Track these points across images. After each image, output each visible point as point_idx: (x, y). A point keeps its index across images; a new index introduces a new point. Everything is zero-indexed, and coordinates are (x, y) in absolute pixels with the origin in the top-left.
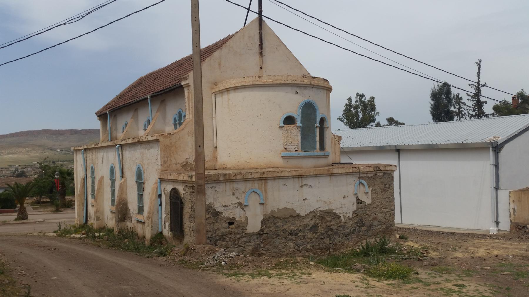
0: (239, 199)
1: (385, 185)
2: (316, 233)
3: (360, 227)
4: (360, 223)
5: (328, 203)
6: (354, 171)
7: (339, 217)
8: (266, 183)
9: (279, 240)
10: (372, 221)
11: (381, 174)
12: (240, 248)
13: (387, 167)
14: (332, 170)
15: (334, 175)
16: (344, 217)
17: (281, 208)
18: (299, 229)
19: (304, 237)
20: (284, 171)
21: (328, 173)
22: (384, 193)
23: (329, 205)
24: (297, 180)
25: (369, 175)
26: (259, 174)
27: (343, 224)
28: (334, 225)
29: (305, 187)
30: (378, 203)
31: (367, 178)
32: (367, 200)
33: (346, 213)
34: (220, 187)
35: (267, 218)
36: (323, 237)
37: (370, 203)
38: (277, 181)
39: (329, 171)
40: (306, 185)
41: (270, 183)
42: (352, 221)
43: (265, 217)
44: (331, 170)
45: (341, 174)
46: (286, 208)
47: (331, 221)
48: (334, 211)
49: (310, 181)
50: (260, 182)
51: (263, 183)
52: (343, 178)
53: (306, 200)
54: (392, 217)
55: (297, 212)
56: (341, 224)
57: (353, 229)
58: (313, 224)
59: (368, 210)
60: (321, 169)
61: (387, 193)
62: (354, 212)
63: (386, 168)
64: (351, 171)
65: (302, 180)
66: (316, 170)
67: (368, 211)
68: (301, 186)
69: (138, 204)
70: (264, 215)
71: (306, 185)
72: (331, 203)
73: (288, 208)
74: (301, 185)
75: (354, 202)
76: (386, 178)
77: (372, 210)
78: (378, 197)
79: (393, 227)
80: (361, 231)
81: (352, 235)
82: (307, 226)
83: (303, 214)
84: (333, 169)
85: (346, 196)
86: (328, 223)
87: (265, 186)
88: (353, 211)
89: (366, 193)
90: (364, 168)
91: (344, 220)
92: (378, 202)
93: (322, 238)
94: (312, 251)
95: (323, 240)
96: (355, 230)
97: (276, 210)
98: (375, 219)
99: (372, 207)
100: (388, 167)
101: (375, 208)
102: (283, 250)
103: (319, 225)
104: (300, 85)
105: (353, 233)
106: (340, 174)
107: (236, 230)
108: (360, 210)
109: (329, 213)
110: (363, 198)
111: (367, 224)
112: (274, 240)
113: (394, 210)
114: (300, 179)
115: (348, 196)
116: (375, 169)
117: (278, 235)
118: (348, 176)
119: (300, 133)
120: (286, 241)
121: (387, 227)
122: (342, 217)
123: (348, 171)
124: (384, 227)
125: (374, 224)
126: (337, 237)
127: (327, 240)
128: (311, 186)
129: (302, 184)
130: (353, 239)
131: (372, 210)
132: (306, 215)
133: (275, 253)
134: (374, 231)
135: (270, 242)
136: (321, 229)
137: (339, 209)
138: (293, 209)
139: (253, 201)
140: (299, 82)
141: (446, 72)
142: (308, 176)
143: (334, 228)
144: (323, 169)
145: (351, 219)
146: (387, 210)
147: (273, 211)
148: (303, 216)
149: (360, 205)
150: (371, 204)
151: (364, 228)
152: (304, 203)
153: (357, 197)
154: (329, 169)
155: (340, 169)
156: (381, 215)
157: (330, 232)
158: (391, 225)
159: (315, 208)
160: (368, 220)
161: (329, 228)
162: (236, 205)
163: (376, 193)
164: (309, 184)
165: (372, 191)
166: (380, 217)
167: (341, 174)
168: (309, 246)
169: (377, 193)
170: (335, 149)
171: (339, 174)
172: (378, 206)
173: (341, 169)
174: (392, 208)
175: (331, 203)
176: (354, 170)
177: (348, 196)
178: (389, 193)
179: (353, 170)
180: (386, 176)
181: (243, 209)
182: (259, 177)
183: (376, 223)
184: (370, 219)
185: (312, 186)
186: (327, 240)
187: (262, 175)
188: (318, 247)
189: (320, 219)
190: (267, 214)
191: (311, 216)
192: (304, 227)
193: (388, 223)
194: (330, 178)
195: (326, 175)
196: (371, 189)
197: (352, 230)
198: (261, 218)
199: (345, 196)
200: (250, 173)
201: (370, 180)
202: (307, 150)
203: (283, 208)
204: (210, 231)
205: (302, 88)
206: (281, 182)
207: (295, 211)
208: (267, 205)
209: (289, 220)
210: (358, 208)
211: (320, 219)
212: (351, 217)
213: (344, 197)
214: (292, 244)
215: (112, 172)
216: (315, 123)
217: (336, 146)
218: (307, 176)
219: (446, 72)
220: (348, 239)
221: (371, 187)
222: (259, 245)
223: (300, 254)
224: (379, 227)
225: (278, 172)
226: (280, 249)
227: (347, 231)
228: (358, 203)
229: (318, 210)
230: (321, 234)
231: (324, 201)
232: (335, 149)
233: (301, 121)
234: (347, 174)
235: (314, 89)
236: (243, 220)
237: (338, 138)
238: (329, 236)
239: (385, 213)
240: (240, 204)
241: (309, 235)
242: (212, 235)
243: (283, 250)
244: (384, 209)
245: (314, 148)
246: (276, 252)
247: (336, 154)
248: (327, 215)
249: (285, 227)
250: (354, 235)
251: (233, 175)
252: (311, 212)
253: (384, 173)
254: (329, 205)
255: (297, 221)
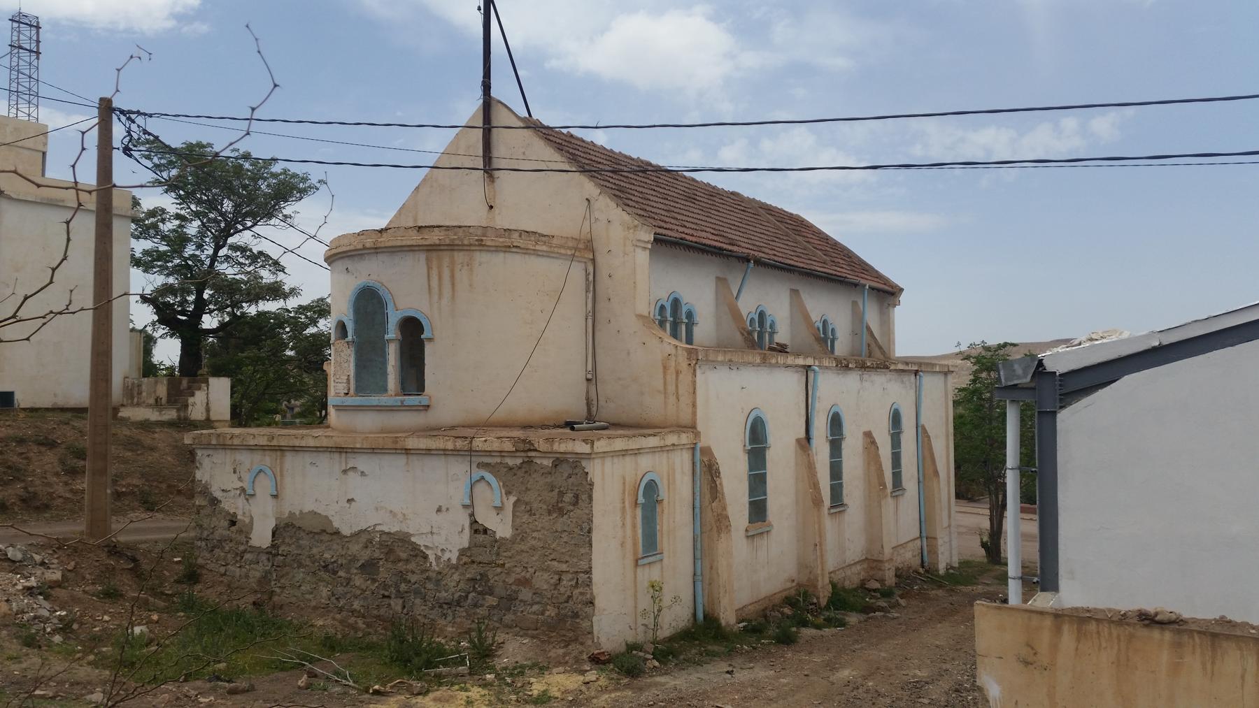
0: (241, 481)
1: (561, 494)
2: (374, 581)
3: (480, 593)
4: (480, 584)
5: (400, 516)
6: (458, 447)
7: (425, 557)
8: (283, 456)
9: (302, 575)
10: (513, 587)
11: (547, 463)
12: (243, 569)
13: (557, 444)
14: (404, 440)
15: (412, 452)
16: (438, 558)
17: (306, 510)
18: (339, 562)
19: (349, 580)
20: (307, 436)
21: (394, 446)
22: (555, 515)
23: (401, 522)
24: (336, 456)
25: (510, 462)
26: (266, 438)
27: (434, 575)
28: (413, 572)
29: (351, 474)
30: (534, 542)
31: (505, 467)
32: (502, 528)
33: (443, 550)
34: (219, 457)
35: (282, 525)
36: (386, 594)
37: (508, 537)
38: (301, 454)
39: (397, 442)
40: (354, 468)
41: (289, 457)
42: (458, 574)
43: (278, 523)
44: (402, 439)
45: (428, 452)
46: (315, 513)
47: (407, 561)
48: (413, 539)
49: (362, 462)
50: (273, 454)
51: (279, 458)
52: (437, 464)
53: (353, 503)
54: (581, 590)
55: (334, 524)
56: (431, 573)
57: (459, 593)
58: (366, 558)
59: (505, 554)
60: (378, 437)
61: (566, 517)
62: (463, 552)
63: (552, 446)
64: (450, 446)
65: (346, 458)
66: (367, 437)
67: (505, 557)
68: (345, 472)
69: (1022, 502)
70: (277, 519)
71: (354, 468)
72: (407, 519)
73: (318, 514)
74: (344, 468)
75: (463, 525)
76: (566, 475)
77: (518, 557)
78: (536, 526)
79: (582, 619)
80: (482, 606)
81: (458, 608)
82: (354, 559)
83: (346, 531)
84: (406, 440)
85: (444, 509)
86: (401, 564)
87: (282, 464)
88: (461, 547)
89: (499, 509)
90: (486, 441)
91: (437, 565)
92: (535, 538)
93: (384, 596)
94: (364, 617)
95: (386, 601)
96: (467, 596)
97: (297, 513)
98: (525, 582)
99: (518, 547)
100: (560, 443)
101: (524, 554)
102: (307, 596)
103: (381, 563)
104: (349, 254)
105: (458, 604)
106: (427, 452)
107: (238, 535)
108: (481, 549)
109: (402, 540)
110: (488, 519)
111: (499, 590)
112: (295, 571)
113: (588, 572)
114: (344, 455)
115: (448, 509)
116: (519, 445)
117: (300, 565)
118: (451, 459)
119: (353, 355)
120: (314, 580)
121: (561, 619)
122: (432, 558)
123: (442, 446)
124: (551, 612)
125: (521, 597)
126: (418, 601)
127: (397, 604)
128: (363, 474)
129: (346, 467)
130: (458, 620)
131: (518, 557)
132: (352, 536)
133: (295, 598)
134: (519, 614)
135: (287, 573)
136: (384, 573)
137: (424, 536)
138: (326, 517)
139: (264, 487)
140: (344, 247)
141: (654, 126)
142: (432, 452)
143: (414, 578)
144: (383, 438)
145: (456, 567)
146: (564, 567)
147: (292, 514)
148: (347, 537)
149: (481, 537)
150: (513, 541)
151: (491, 601)
152: (349, 508)
153: (472, 515)
154: (396, 437)
155: (421, 439)
156: (546, 576)
157: (403, 587)
158: (576, 615)
159: (371, 523)
160: (504, 581)
161: (402, 576)
162: (238, 492)
163: (530, 512)
164: (361, 468)
165: (515, 505)
166: (542, 581)
167: (428, 452)
168: (356, 605)
169: (535, 514)
170: (677, 386)
171: (424, 452)
172: (534, 549)
173: (425, 440)
174: (583, 565)
175: (407, 519)
176: (457, 444)
177: (448, 509)
178: (574, 521)
179: (456, 445)
180: (565, 470)
181: (247, 500)
182: (265, 443)
183: (526, 594)
184: (510, 580)
185: (367, 473)
186: (397, 604)
187: (270, 441)
188: (375, 612)
189: (383, 550)
190: (282, 517)
191: (364, 538)
192: (350, 561)
193: (566, 605)
194: (408, 458)
195: (315, 449)
196: (513, 499)
197: (456, 596)
198: (272, 524)
199: (440, 506)
200: (252, 437)
201: (515, 475)
202: (368, 392)
203: (309, 511)
204: (207, 529)
205: (356, 259)
206: (308, 458)
207: (331, 522)
208: (282, 499)
209: (322, 539)
210: (473, 545)
211: (383, 550)
212: (454, 561)
213: (439, 510)
214: (325, 592)
215: (896, 419)
216: (385, 331)
217: (681, 377)
218: (354, 451)
219: (654, 126)
220: (445, 616)
221: (514, 493)
222: (269, 572)
223: (338, 615)
224: (535, 608)
225: (297, 438)
226: (303, 594)
227: (444, 594)
228: (476, 531)
229: (378, 528)
230: (383, 585)
231: (391, 512)
232: (677, 386)
233: (355, 330)
234: (445, 452)
235: (381, 257)
236: (247, 520)
237: (686, 354)
238: (400, 595)
239: (560, 573)
240: (243, 490)
241: (358, 581)
242: (208, 536)
243: (307, 596)
244: (555, 563)
245: (384, 389)
246: (295, 596)
247: (681, 399)
248: (400, 544)
249: (315, 551)
250: (462, 609)
251: (229, 437)
252: (361, 531)
253: (558, 458)
254: (401, 522)
255: (338, 544)
